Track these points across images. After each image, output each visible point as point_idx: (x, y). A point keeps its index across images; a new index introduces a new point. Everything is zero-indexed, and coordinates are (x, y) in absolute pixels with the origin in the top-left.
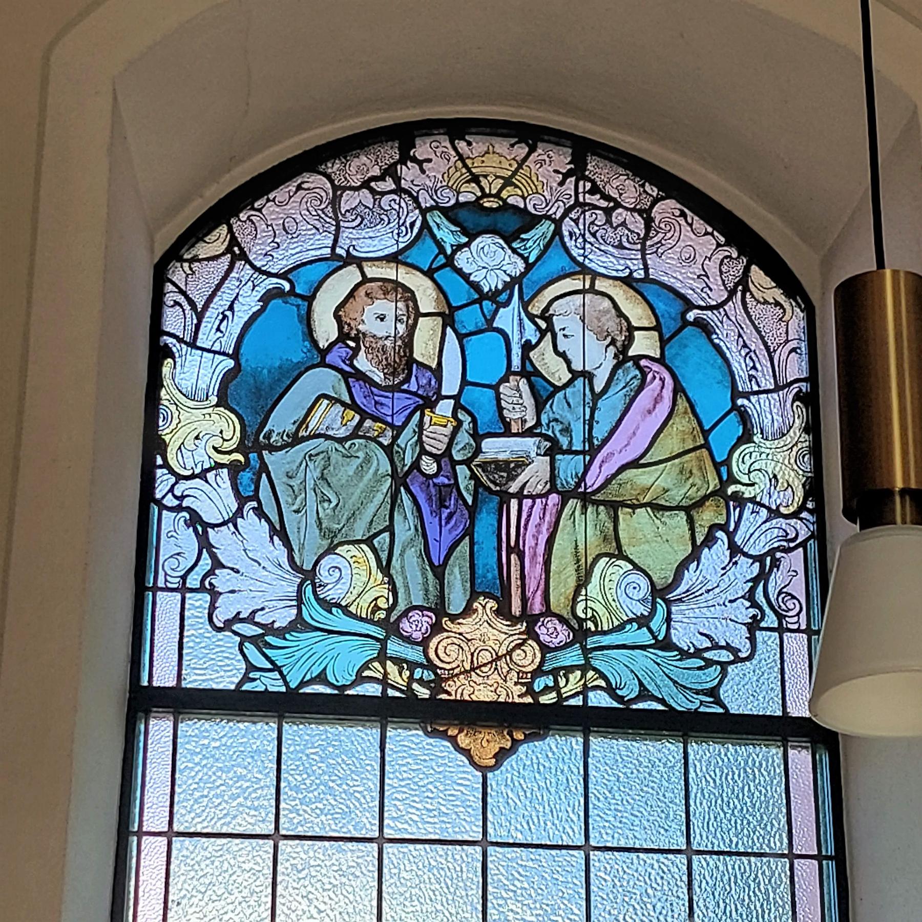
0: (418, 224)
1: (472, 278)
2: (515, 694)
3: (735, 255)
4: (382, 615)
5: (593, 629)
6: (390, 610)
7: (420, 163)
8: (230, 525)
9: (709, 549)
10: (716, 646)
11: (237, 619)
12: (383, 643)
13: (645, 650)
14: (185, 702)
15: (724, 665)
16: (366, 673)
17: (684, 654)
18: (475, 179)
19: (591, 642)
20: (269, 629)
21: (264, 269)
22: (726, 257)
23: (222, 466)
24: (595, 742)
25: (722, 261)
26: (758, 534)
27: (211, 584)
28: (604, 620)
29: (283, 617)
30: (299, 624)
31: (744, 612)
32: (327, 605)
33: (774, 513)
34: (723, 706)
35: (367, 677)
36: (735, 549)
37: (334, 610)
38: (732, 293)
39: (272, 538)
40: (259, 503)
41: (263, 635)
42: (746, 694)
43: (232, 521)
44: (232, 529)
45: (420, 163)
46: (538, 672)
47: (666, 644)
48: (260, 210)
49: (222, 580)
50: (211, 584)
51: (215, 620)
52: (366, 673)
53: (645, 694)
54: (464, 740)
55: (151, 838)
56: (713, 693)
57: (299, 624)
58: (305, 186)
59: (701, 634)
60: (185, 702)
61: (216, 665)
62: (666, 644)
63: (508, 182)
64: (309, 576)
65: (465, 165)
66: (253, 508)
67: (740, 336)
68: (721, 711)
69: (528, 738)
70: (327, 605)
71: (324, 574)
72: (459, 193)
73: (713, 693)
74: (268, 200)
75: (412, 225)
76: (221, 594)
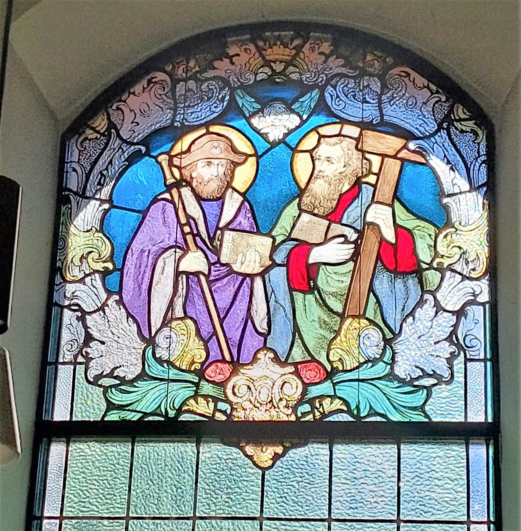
0: (227, 98)
1: (262, 132)
2: (284, 415)
3: (444, 99)
4: (198, 366)
5: (341, 368)
6: (202, 364)
7: (231, 58)
8: (101, 312)
9: (421, 307)
10: (426, 375)
11: (101, 376)
12: (197, 385)
13: (470, 168)
14: (76, 431)
15: (429, 389)
16: (272, 64)
17: (403, 382)
18: (267, 63)
19: (336, 379)
20: (123, 381)
21: (128, 140)
22: (437, 102)
23: (98, 271)
24: (338, 448)
25: (434, 105)
26: (453, 293)
27: (86, 352)
28: (348, 363)
29: (131, 371)
30: (143, 376)
31: (446, 349)
32: (159, 361)
33: (465, 278)
34: (427, 416)
35: (186, 410)
36: (439, 308)
37: (432, 373)
38: (440, 127)
39: (127, 318)
40: (121, 297)
41: (119, 385)
42: (445, 407)
43: (101, 309)
44: (102, 314)
45: (231, 58)
46: (301, 402)
47: (391, 376)
48: (125, 101)
49: (94, 349)
50: (86, 352)
51: (89, 377)
52: (272, 64)
53: (373, 412)
54: (249, 450)
55: (55, 516)
56: (422, 408)
57: (143, 376)
58: (154, 80)
59: (416, 367)
60: (76, 431)
61: (91, 407)
62: (391, 376)
63: (288, 64)
64: (150, 341)
65: (261, 55)
66: (116, 300)
67: (445, 156)
68: (427, 420)
69: (294, 446)
70: (159, 361)
71: (160, 339)
72: (256, 74)
73: (422, 408)
74: (130, 93)
75: (223, 98)
76: (93, 359)
